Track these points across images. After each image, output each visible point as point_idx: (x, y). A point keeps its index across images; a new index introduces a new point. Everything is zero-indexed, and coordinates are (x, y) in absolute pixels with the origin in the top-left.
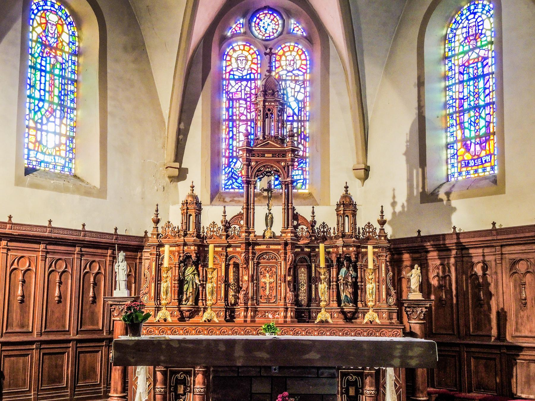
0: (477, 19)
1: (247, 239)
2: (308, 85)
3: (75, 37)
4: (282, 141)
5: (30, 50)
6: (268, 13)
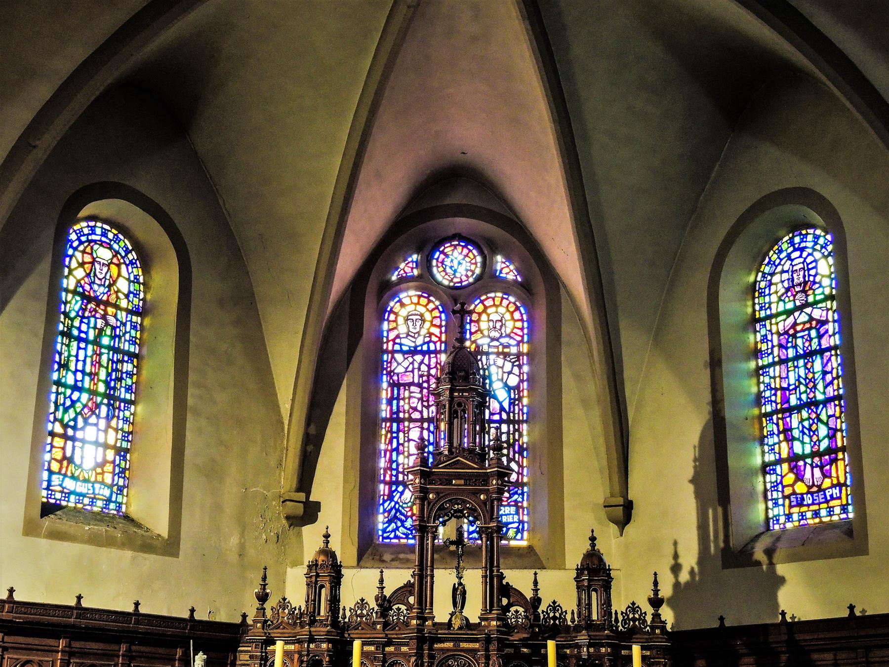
0: (805, 259)
1: (420, 629)
2: (525, 362)
3: (139, 283)
4: (482, 457)
5: (63, 306)
6: (459, 245)
